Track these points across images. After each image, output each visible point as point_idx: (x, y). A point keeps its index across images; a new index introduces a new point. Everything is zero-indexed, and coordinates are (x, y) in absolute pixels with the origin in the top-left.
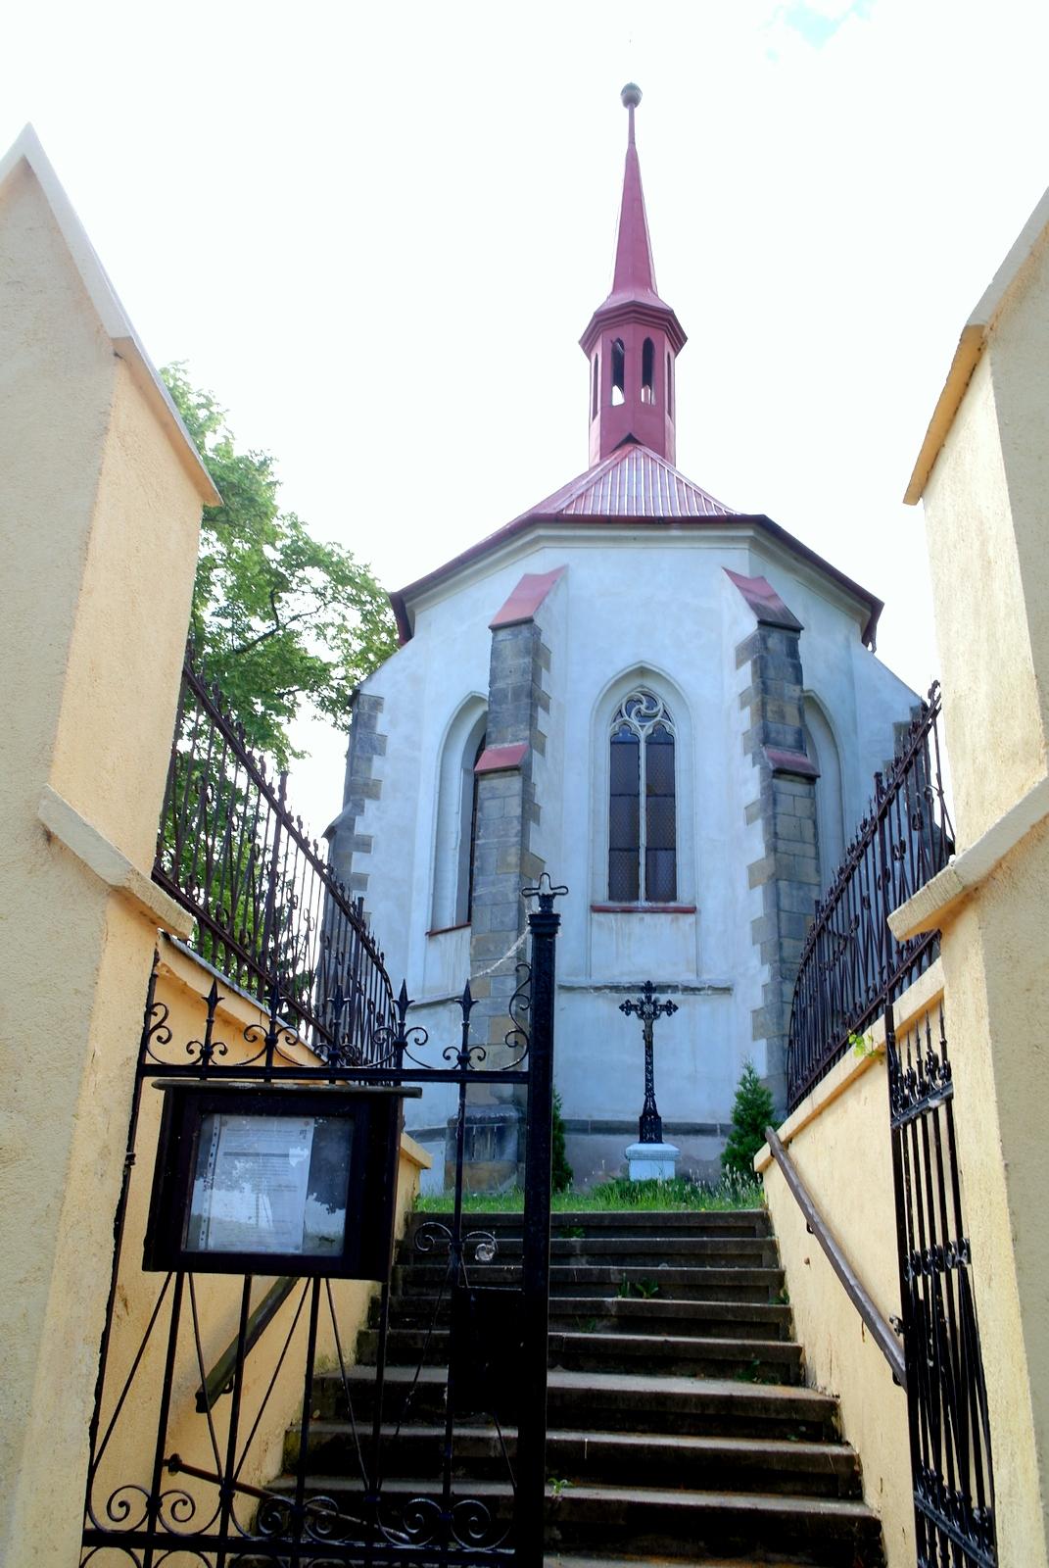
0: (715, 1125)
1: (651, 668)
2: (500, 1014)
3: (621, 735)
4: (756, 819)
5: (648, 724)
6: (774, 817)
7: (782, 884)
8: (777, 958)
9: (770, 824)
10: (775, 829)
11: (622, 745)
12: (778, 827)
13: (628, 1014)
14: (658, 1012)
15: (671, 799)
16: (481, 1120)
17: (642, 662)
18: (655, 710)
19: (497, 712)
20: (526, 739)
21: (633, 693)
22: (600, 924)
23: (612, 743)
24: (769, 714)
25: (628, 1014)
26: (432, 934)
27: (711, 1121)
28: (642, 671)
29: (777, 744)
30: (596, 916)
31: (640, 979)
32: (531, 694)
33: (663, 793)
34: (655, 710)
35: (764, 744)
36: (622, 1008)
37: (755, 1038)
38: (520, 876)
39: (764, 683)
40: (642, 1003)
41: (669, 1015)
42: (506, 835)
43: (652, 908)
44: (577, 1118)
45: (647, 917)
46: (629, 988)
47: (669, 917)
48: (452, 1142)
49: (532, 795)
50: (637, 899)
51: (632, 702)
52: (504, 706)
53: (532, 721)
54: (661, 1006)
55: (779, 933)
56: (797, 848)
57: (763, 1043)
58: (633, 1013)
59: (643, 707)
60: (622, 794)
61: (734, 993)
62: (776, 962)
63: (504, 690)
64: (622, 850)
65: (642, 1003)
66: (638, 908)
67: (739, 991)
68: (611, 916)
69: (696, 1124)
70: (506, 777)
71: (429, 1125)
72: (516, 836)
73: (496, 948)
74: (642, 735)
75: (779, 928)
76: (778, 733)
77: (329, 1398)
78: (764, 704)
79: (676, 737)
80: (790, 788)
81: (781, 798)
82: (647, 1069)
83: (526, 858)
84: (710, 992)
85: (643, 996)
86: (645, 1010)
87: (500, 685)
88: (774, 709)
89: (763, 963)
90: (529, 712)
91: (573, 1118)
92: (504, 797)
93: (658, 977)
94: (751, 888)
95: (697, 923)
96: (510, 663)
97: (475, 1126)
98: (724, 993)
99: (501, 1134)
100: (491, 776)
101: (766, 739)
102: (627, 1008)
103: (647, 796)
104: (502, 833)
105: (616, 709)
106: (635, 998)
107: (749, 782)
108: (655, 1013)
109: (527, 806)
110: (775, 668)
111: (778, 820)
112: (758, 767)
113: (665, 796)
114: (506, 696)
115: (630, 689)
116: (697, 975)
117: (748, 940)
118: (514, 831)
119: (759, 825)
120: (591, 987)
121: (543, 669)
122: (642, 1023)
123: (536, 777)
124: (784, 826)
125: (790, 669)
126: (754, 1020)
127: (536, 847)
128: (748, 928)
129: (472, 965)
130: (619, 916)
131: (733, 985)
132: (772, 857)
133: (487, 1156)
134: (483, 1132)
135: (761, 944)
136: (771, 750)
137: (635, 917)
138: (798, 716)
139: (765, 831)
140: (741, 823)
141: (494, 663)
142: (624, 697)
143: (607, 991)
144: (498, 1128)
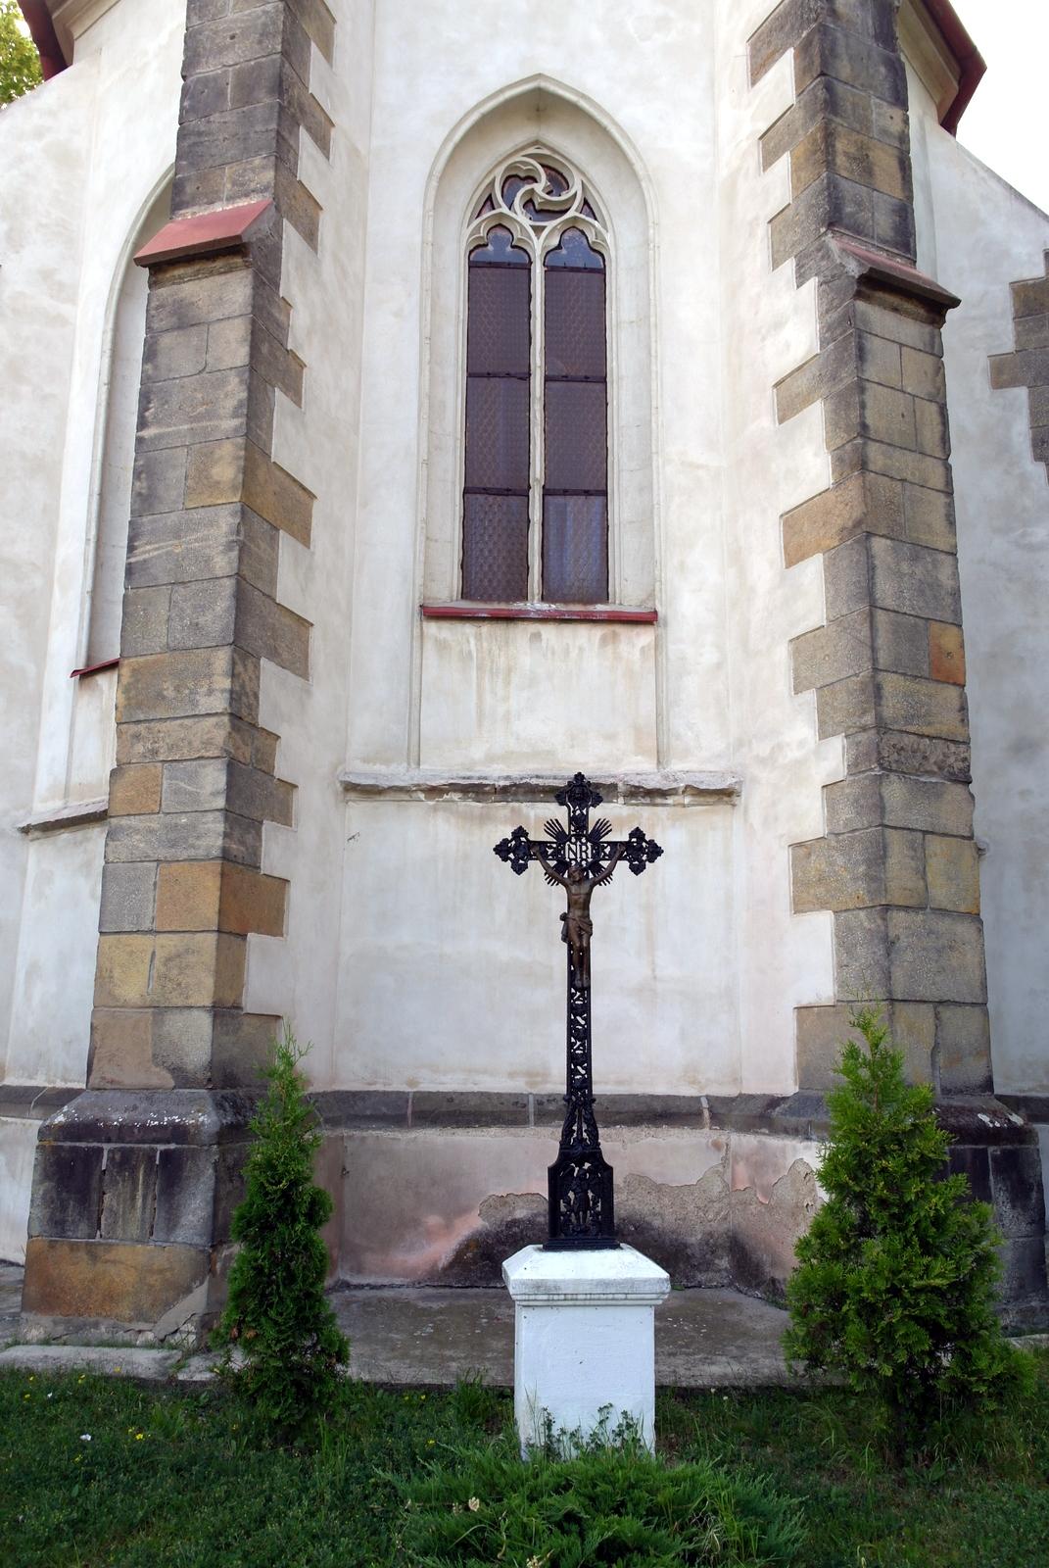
0: (697, 1099)
1: (561, 92)
2: (185, 855)
3: (490, 248)
4: (806, 401)
5: (550, 224)
6: (860, 387)
7: (879, 545)
8: (869, 719)
9: (848, 405)
10: (862, 416)
11: (494, 273)
12: (868, 413)
13: (519, 869)
14: (605, 864)
15: (598, 387)
16: (123, 1132)
17: (539, 76)
18: (565, 196)
19: (200, 134)
20: (266, 189)
21: (518, 158)
22: (442, 646)
23: (473, 266)
24: (841, 160)
25: (519, 869)
26: (86, 674)
27: (687, 1091)
28: (539, 103)
29: (858, 230)
30: (432, 628)
31: (562, 768)
32: (280, 87)
33: (584, 376)
34: (565, 196)
35: (830, 225)
36: (502, 850)
37: (799, 906)
38: (243, 513)
39: (829, 88)
40: (562, 837)
41: (637, 869)
42: (210, 415)
43: (563, 613)
44: (380, 1087)
45: (549, 632)
46: (505, 790)
47: (598, 632)
48: (45, 1211)
49: (283, 328)
50: (524, 597)
51: (514, 179)
52: (216, 117)
53: (283, 156)
54: (613, 844)
55: (874, 660)
56: (905, 463)
57: (823, 923)
58: (535, 867)
59: (539, 188)
60: (492, 369)
61: (741, 801)
62: (864, 729)
63: (215, 79)
64: (490, 489)
65: (562, 837)
66: (528, 612)
67: (755, 800)
68: (468, 629)
69: (653, 1097)
70: (211, 273)
71: (65, 1080)
72: (235, 415)
73: (177, 689)
74: (538, 246)
75: (874, 649)
76: (859, 204)
77: (877, 71)
78: (829, 136)
79: (611, 254)
80: (887, 323)
81: (873, 344)
82: (571, 1023)
83: (261, 473)
84: (687, 800)
85: (560, 813)
86: (569, 855)
87: (208, 69)
88: (852, 150)
89: (824, 733)
90: (274, 126)
91: (372, 1088)
92: (209, 324)
93: (594, 769)
94: (790, 562)
95: (658, 645)
96: (231, 16)
97: (107, 1147)
98: (720, 801)
99: (170, 1173)
100: (178, 272)
101: (834, 219)
102: (517, 851)
103: (547, 379)
104: (202, 409)
105: (480, 193)
106: (542, 817)
107: (792, 322)
108: (595, 866)
109: (265, 349)
110: (851, 58)
111: (869, 398)
112: (812, 283)
113: (586, 379)
114: (221, 94)
115: (509, 144)
116: (659, 762)
117: (783, 682)
118: (230, 404)
119: (815, 416)
120: (420, 788)
121: (314, 48)
122: (557, 899)
123: (291, 285)
124: (881, 410)
125: (883, 70)
126: (796, 863)
127: (291, 446)
128: (782, 653)
129: (120, 734)
130: (486, 628)
131: (740, 783)
132: (853, 487)
133: (134, 1230)
134: (125, 1163)
135: (817, 689)
136: (845, 239)
137: (521, 632)
138: (899, 176)
139: (834, 423)
140: (765, 422)
141: (196, 21)
142: (500, 163)
143: (456, 796)
144: (165, 1154)
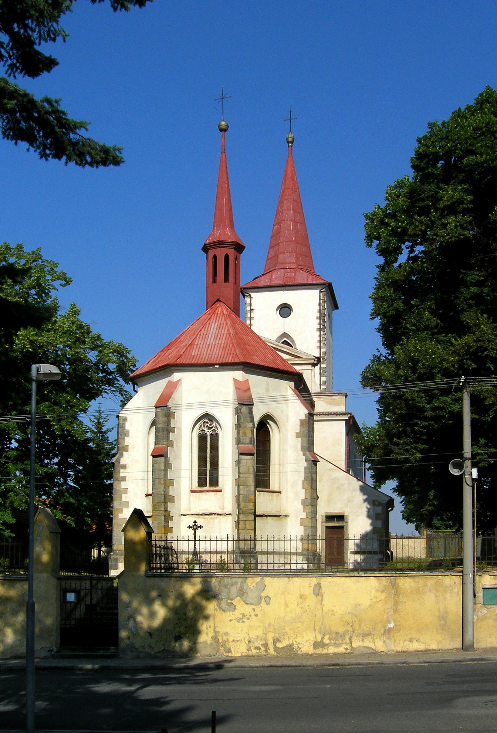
24: (241, 434)
32: (167, 430)
56: (247, 475)
74: (208, 433)
